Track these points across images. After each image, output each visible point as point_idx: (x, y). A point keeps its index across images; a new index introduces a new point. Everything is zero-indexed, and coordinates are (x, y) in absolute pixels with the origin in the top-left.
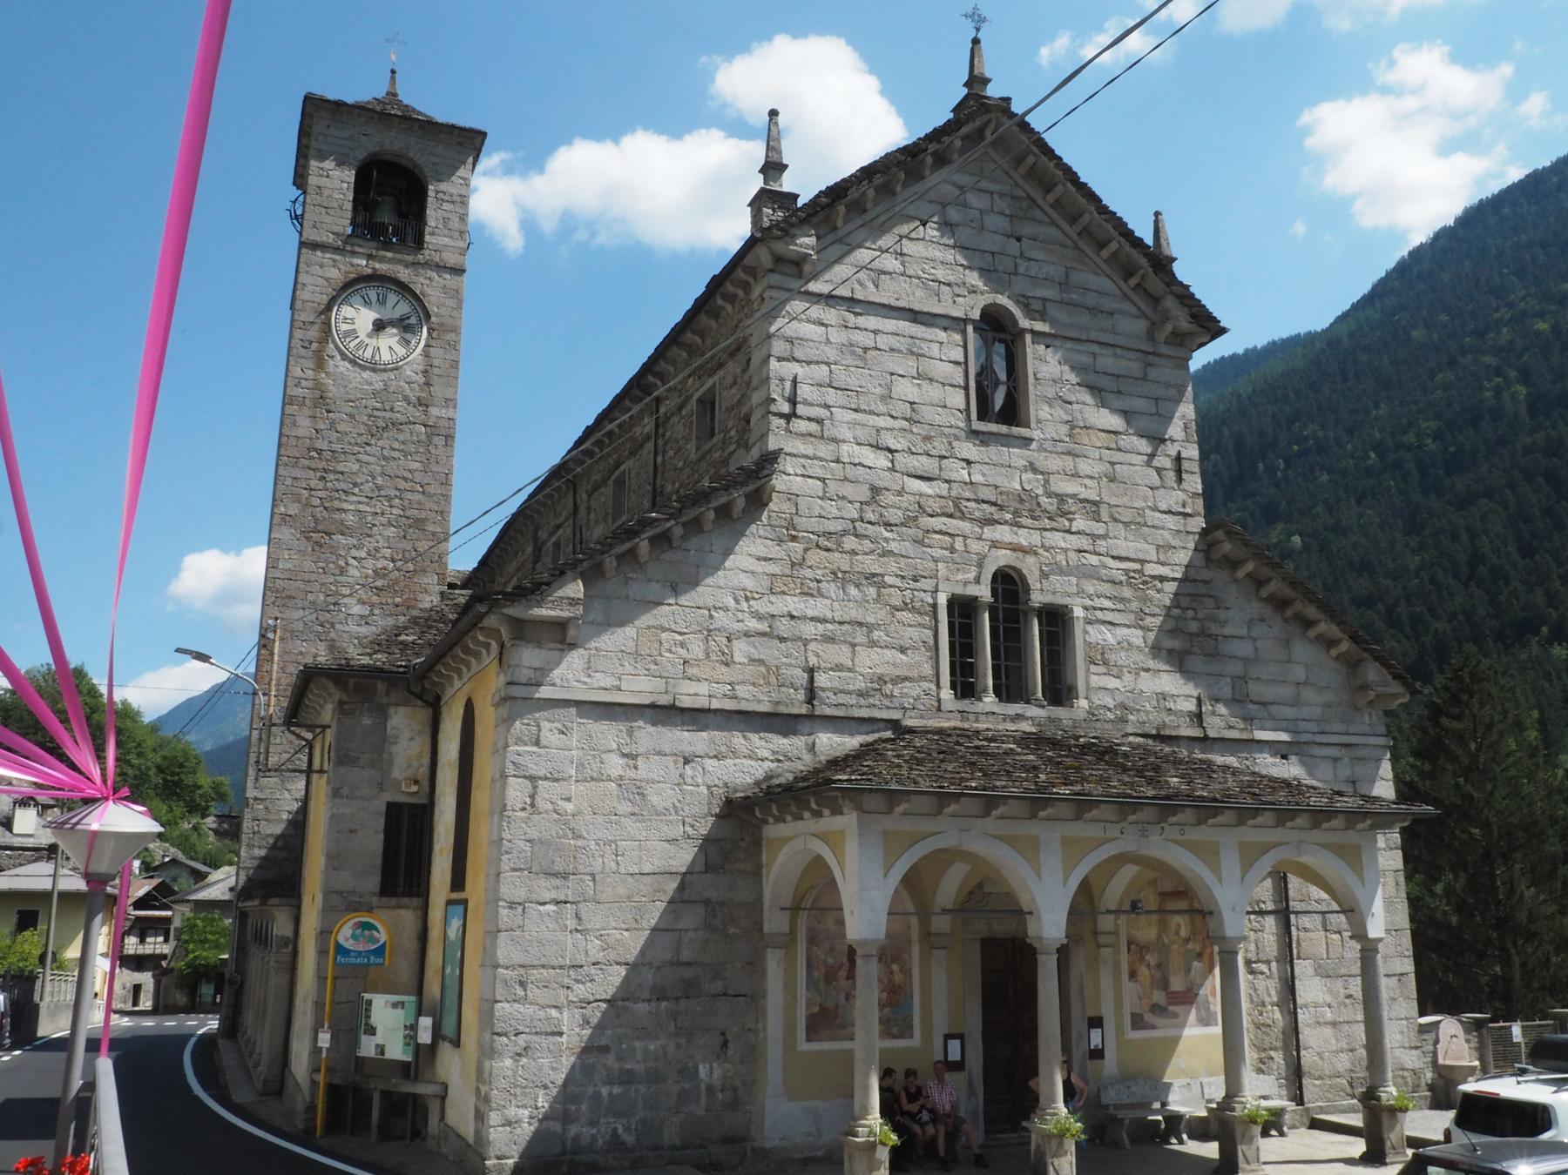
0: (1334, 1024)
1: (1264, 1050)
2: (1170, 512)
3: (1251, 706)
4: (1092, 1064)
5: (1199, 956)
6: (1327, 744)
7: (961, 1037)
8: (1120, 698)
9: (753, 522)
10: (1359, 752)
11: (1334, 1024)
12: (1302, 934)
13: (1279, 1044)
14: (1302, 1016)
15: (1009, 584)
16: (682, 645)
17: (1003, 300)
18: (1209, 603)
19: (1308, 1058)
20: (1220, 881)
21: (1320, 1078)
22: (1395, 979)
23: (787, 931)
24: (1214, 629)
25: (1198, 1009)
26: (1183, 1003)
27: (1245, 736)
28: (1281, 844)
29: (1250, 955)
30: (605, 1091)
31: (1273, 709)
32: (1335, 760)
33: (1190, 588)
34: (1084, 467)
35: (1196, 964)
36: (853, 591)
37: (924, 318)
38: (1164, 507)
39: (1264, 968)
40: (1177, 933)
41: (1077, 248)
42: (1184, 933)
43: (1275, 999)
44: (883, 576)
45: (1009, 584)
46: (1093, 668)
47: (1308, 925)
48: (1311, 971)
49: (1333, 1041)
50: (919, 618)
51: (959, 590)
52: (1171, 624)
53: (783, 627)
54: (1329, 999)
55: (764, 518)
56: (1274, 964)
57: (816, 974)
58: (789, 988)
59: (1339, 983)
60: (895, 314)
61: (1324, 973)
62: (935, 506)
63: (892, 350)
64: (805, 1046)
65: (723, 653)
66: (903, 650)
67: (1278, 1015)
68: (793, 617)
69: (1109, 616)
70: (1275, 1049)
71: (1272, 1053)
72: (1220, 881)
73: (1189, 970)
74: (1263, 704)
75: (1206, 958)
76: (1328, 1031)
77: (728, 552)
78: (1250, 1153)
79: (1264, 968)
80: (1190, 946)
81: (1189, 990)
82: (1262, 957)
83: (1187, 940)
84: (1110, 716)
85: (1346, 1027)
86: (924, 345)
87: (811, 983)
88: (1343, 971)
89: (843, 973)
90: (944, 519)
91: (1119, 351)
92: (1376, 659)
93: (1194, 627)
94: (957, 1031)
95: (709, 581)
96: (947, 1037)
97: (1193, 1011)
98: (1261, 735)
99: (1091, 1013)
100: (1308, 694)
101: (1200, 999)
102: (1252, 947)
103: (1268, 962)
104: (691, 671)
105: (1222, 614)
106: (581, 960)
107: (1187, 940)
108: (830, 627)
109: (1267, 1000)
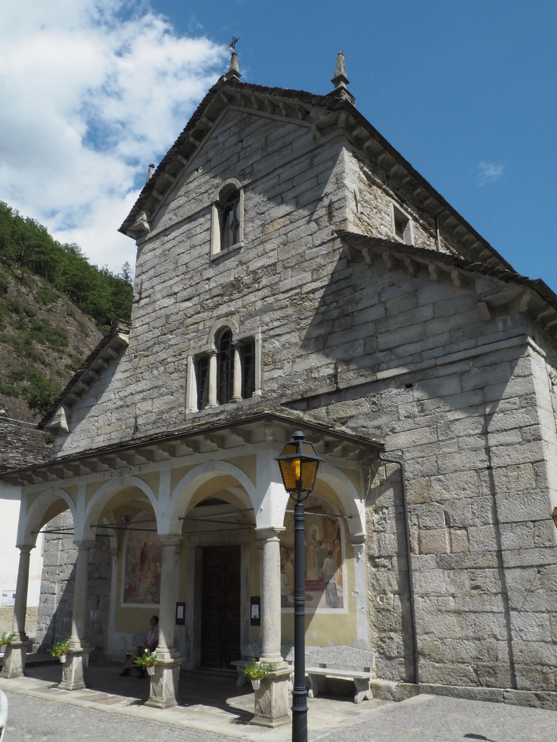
0: (458, 613)
1: (385, 631)
2: (323, 243)
3: (380, 355)
4: (251, 628)
5: (330, 553)
6: (452, 363)
7: (183, 604)
8: (281, 382)
9: (122, 356)
10: (488, 360)
11: (458, 613)
12: (423, 532)
13: (398, 627)
14: (419, 603)
15: (224, 337)
16: (97, 421)
17: (229, 181)
18: (347, 292)
19: (422, 641)
20: (157, 498)
21: (440, 661)
22: (532, 572)
23: (117, 547)
24: (350, 309)
25: (327, 594)
26: (317, 590)
27: (369, 379)
28: (197, 465)
29: (372, 552)
30: (65, 619)
31: (400, 351)
32: (462, 374)
33: (334, 288)
34: (269, 246)
35: (327, 560)
36: (155, 372)
37: (195, 216)
38: (318, 242)
39: (386, 562)
40: (314, 538)
41: (274, 120)
42: (318, 537)
43: (396, 588)
44: (166, 359)
45: (224, 337)
46: (266, 368)
47: (429, 524)
48: (433, 564)
49: (458, 629)
50: (180, 375)
51: (197, 352)
52: (320, 318)
53: (129, 401)
54: (452, 590)
55: (126, 353)
56: (395, 559)
57: (129, 568)
58: (119, 574)
59: (465, 576)
60: (182, 224)
61: (445, 564)
62: (192, 311)
63: (180, 242)
64: (123, 605)
65: (109, 420)
66: (172, 394)
67: (398, 603)
68: (132, 394)
69: (278, 331)
70: (395, 631)
71: (392, 634)
72: (157, 498)
73: (321, 565)
74: (391, 349)
75: (335, 555)
76: (452, 619)
77: (113, 374)
78: (157, 689)
79: (386, 562)
80: (323, 547)
81: (321, 580)
82: (383, 553)
83: (321, 542)
84: (275, 395)
85: (472, 616)
86: (193, 232)
87: (127, 574)
88: (468, 564)
89: (138, 568)
90: (196, 316)
91: (294, 162)
92: (484, 272)
93: (335, 314)
94: (182, 601)
95: (107, 390)
96: (178, 604)
97: (324, 596)
98: (382, 375)
99: (254, 594)
100: (435, 326)
101: (329, 586)
102: (375, 546)
103: (390, 557)
104: (99, 432)
105: (358, 295)
106: (63, 563)
107: (321, 542)
108: (145, 393)
109: (388, 588)
